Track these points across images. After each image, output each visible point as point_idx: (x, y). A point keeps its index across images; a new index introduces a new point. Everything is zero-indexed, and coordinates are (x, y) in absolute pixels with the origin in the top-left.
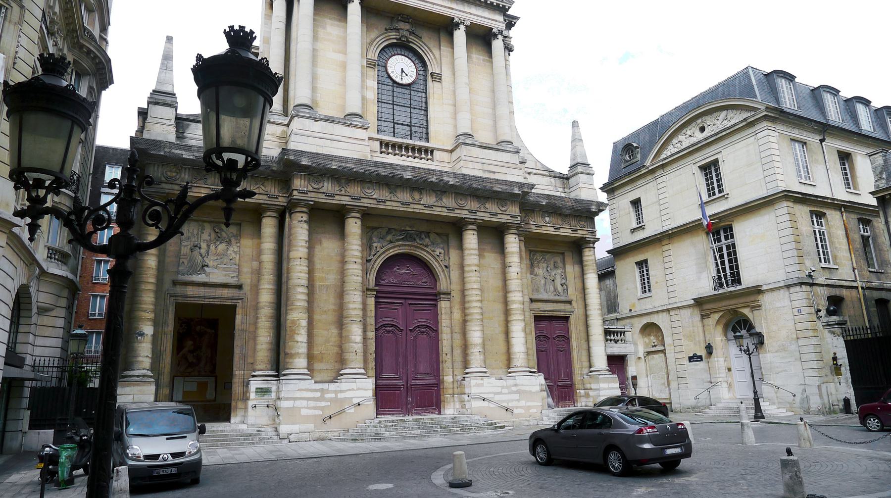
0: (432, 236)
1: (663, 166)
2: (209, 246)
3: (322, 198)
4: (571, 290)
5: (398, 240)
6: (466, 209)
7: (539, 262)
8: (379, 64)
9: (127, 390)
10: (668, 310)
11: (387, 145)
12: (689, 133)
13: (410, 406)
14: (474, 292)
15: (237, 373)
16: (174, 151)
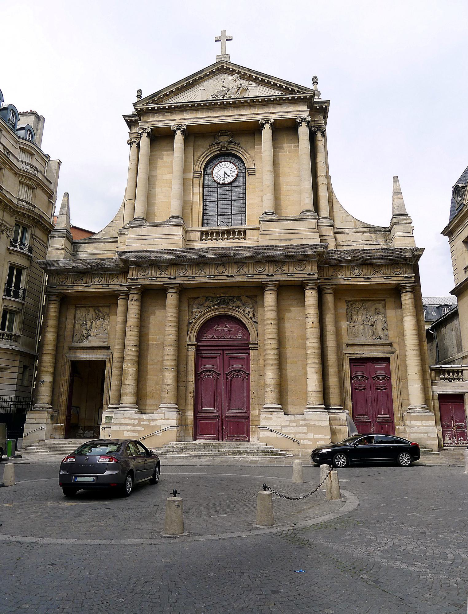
0: (244, 299)
2: (92, 323)
3: (147, 282)
4: (391, 334)
5: (214, 305)
6: (264, 273)
7: (358, 311)
8: (204, 174)
9: (32, 416)
11: (207, 233)
13: (223, 434)
14: (269, 342)
16: (60, 265)
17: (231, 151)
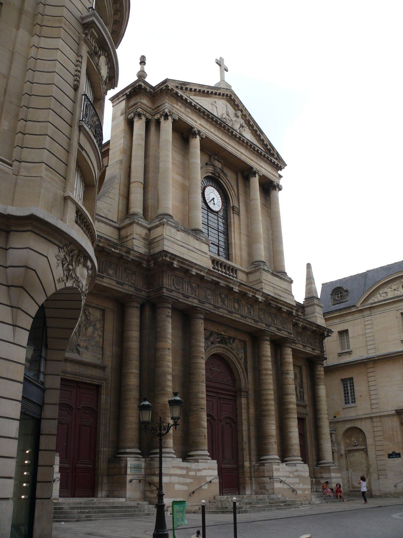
1: (370, 308)
10: (371, 418)
12: (393, 287)
15: (102, 449)
17: (220, 180)
